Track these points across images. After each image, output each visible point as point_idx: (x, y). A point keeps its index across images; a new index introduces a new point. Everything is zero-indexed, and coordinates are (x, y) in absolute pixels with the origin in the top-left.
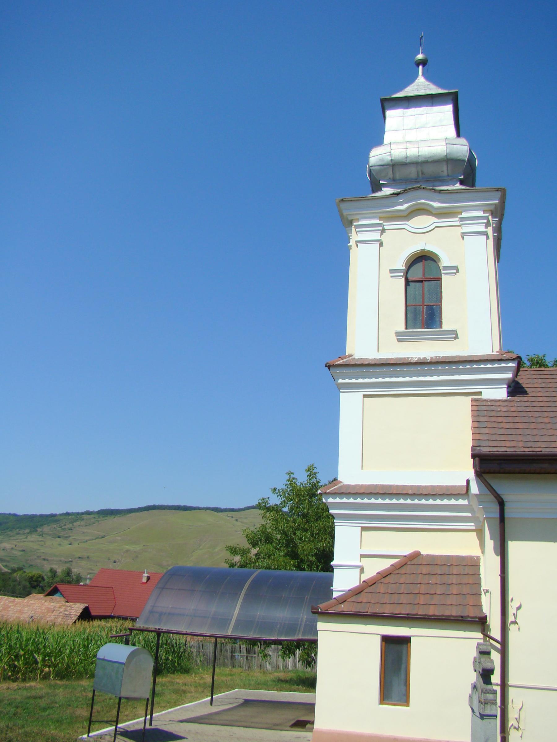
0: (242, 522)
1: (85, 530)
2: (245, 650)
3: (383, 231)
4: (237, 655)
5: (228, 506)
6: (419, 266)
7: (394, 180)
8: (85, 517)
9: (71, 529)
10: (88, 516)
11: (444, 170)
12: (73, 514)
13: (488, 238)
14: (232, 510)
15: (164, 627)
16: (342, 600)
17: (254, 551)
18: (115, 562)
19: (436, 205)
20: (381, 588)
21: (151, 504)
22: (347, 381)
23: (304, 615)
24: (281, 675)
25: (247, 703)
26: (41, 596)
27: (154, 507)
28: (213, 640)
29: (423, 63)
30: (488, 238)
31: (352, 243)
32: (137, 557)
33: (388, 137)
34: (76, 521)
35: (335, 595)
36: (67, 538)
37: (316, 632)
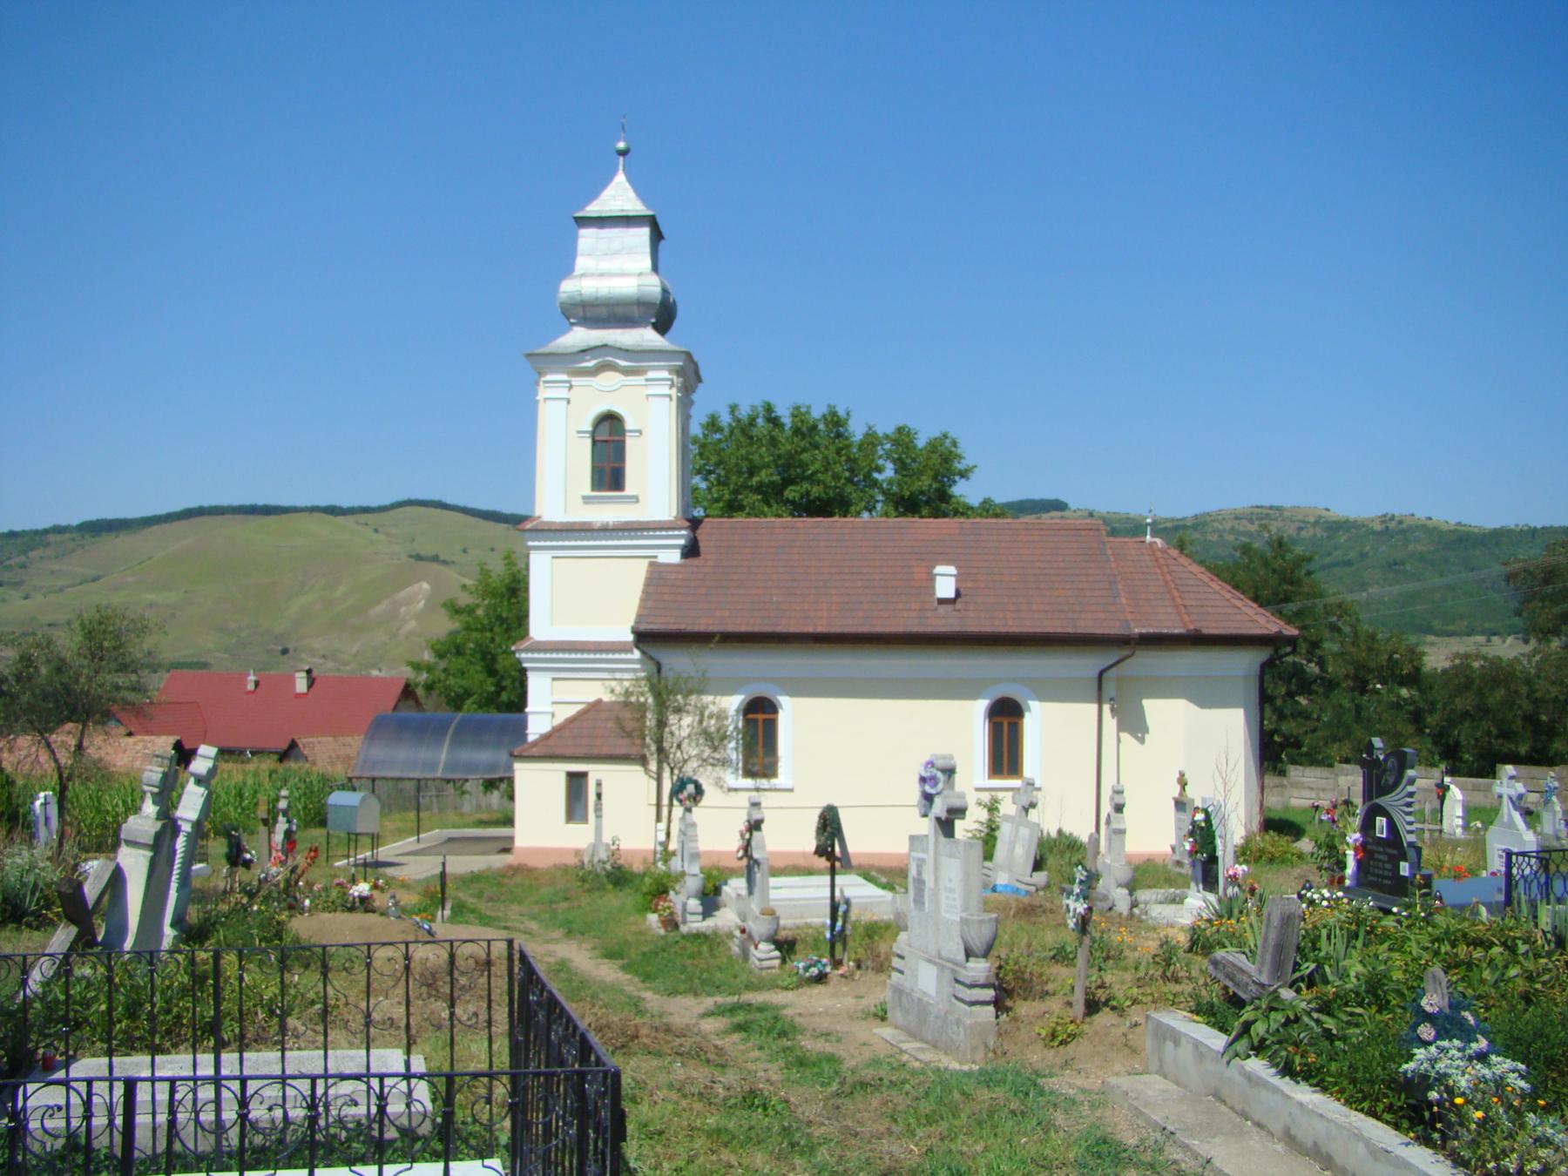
0: (388, 534)
1: (56, 567)
3: (571, 387)
5: (356, 503)
6: (606, 425)
8: (52, 538)
9: (23, 566)
10: (59, 537)
11: (636, 311)
12: (24, 534)
14: (366, 510)
15: (376, 774)
16: (535, 743)
19: (622, 363)
21: (194, 503)
23: (503, 756)
24: (484, 816)
25: (451, 840)
29: (623, 153)
33: (581, 263)
34: (33, 549)
35: (531, 738)
36: (17, 585)
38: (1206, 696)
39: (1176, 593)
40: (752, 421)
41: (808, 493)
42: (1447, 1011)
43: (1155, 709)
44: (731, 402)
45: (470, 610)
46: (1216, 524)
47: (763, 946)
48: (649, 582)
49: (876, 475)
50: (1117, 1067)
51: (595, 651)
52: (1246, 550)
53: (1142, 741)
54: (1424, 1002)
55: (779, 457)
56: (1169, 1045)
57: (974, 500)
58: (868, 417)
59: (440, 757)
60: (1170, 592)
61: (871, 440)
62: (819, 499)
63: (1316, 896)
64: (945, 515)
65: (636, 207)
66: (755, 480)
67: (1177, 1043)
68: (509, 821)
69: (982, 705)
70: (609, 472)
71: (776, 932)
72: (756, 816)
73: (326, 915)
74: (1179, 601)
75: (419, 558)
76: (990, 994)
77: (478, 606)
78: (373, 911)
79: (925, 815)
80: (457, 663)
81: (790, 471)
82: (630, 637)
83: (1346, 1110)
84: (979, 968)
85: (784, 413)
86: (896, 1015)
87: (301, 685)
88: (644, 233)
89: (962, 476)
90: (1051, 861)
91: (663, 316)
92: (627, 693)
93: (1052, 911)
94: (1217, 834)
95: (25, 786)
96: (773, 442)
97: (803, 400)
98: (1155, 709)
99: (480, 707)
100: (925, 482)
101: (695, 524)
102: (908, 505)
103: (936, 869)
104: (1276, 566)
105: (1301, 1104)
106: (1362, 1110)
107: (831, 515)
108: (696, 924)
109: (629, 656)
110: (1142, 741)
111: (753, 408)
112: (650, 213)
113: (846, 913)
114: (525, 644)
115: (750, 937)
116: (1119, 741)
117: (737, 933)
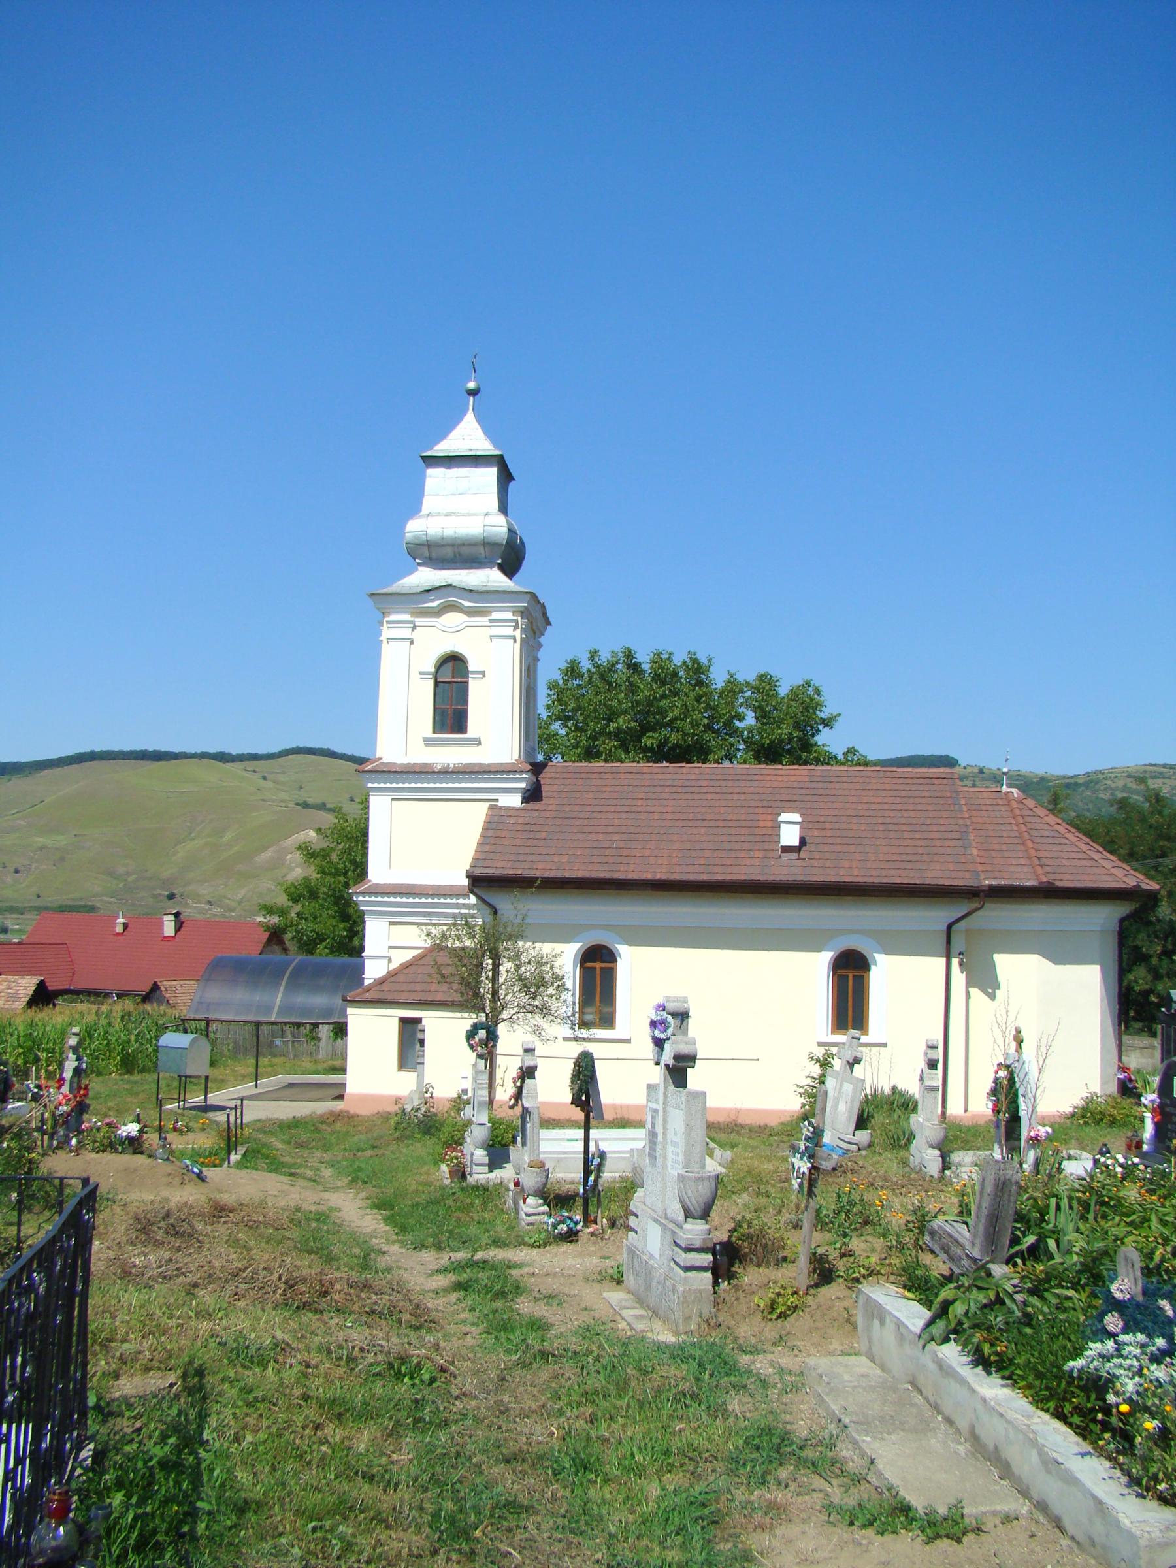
2: (288, 1032)
3: (414, 628)
4: (278, 1041)
5: (246, 750)
6: (450, 665)
7: (430, 559)
13: (515, 641)
14: (255, 757)
17: (298, 908)
18: (17, 871)
19: (466, 604)
20: (401, 978)
21: (86, 749)
22: (376, 785)
23: (338, 1001)
25: (291, 1085)
26: (772, 1124)
27: (92, 756)
28: (204, 1024)
29: (474, 393)
30: (515, 641)
31: (383, 638)
32: (62, 859)
33: (428, 504)
35: (366, 982)
37: (346, 1016)
38: (1060, 951)
39: (1029, 844)
40: (612, 666)
41: (666, 740)
42: (1140, 1298)
43: (1005, 963)
44: (593, 647)
45: (324, 854)
46: (1108, 782)
47: (531, 1200)
48: (488, 826)
49: (737, 723)
50: (835, 1345)
51: (433, 896)
52: (1123, 804)
53: (992, 997)
54: (1113, 1288)
55: (638, 703)
56: (876, 1323)
57: (838, 750)
58: (731, 662)
59: (275, 1001)
60: (1024, 844)
61: (733, 688)
62: (677, 746)
63: (1109, 1162)
64: (805, 763)
65: (484, 446)
66: (613, 726)
67: (882, 1322)
68: (343, 1070)
69: (825, 958)
70: (451, 716)
71: (545, 1185)
72: (529, 1062)
73: (94, 1155)
74: (1033, 853)
75: (306, 805)
76: (707, 1259)
77: (332, 850)
78: (142, 1153)
79: (657, 1063)
80: (310, 907)
81: (649, 718)
82: (465, 882)
83: (1031, 1409)
84: (695, 1230)
85: (644, 659)
86: (629, 1279)
87: (169, 928)
88: (492, 472)
89: (826, 725)
90: (879, 1119)
91: (511, 557)
92: (444, 937)
93: (853, 1171)
94: (1020, 1092)
95: (1051, 1127)
96: (632, 688)
97: (664, 646)
98: (1005, 963)
99: (332, 952)
100: (785, 730)
101: (537, 769)
102: (769, 753)
103: (665, 1120)
104: (1153, 821)
105: (984, 1400)
106: (1047, 1411)
107: (689, 761)
108: (480, 1175)
109: (467, 901)
110: (992, 997)
111: (614, 654)
112: (498, 453)
113: (600, 1165)
114: (363, 887)
115: (523, 1190)
116: (968, 996)
117: (511, 1186)
